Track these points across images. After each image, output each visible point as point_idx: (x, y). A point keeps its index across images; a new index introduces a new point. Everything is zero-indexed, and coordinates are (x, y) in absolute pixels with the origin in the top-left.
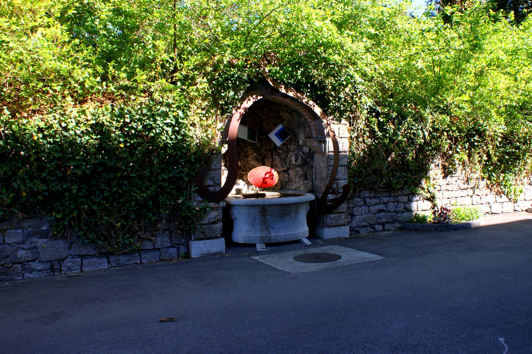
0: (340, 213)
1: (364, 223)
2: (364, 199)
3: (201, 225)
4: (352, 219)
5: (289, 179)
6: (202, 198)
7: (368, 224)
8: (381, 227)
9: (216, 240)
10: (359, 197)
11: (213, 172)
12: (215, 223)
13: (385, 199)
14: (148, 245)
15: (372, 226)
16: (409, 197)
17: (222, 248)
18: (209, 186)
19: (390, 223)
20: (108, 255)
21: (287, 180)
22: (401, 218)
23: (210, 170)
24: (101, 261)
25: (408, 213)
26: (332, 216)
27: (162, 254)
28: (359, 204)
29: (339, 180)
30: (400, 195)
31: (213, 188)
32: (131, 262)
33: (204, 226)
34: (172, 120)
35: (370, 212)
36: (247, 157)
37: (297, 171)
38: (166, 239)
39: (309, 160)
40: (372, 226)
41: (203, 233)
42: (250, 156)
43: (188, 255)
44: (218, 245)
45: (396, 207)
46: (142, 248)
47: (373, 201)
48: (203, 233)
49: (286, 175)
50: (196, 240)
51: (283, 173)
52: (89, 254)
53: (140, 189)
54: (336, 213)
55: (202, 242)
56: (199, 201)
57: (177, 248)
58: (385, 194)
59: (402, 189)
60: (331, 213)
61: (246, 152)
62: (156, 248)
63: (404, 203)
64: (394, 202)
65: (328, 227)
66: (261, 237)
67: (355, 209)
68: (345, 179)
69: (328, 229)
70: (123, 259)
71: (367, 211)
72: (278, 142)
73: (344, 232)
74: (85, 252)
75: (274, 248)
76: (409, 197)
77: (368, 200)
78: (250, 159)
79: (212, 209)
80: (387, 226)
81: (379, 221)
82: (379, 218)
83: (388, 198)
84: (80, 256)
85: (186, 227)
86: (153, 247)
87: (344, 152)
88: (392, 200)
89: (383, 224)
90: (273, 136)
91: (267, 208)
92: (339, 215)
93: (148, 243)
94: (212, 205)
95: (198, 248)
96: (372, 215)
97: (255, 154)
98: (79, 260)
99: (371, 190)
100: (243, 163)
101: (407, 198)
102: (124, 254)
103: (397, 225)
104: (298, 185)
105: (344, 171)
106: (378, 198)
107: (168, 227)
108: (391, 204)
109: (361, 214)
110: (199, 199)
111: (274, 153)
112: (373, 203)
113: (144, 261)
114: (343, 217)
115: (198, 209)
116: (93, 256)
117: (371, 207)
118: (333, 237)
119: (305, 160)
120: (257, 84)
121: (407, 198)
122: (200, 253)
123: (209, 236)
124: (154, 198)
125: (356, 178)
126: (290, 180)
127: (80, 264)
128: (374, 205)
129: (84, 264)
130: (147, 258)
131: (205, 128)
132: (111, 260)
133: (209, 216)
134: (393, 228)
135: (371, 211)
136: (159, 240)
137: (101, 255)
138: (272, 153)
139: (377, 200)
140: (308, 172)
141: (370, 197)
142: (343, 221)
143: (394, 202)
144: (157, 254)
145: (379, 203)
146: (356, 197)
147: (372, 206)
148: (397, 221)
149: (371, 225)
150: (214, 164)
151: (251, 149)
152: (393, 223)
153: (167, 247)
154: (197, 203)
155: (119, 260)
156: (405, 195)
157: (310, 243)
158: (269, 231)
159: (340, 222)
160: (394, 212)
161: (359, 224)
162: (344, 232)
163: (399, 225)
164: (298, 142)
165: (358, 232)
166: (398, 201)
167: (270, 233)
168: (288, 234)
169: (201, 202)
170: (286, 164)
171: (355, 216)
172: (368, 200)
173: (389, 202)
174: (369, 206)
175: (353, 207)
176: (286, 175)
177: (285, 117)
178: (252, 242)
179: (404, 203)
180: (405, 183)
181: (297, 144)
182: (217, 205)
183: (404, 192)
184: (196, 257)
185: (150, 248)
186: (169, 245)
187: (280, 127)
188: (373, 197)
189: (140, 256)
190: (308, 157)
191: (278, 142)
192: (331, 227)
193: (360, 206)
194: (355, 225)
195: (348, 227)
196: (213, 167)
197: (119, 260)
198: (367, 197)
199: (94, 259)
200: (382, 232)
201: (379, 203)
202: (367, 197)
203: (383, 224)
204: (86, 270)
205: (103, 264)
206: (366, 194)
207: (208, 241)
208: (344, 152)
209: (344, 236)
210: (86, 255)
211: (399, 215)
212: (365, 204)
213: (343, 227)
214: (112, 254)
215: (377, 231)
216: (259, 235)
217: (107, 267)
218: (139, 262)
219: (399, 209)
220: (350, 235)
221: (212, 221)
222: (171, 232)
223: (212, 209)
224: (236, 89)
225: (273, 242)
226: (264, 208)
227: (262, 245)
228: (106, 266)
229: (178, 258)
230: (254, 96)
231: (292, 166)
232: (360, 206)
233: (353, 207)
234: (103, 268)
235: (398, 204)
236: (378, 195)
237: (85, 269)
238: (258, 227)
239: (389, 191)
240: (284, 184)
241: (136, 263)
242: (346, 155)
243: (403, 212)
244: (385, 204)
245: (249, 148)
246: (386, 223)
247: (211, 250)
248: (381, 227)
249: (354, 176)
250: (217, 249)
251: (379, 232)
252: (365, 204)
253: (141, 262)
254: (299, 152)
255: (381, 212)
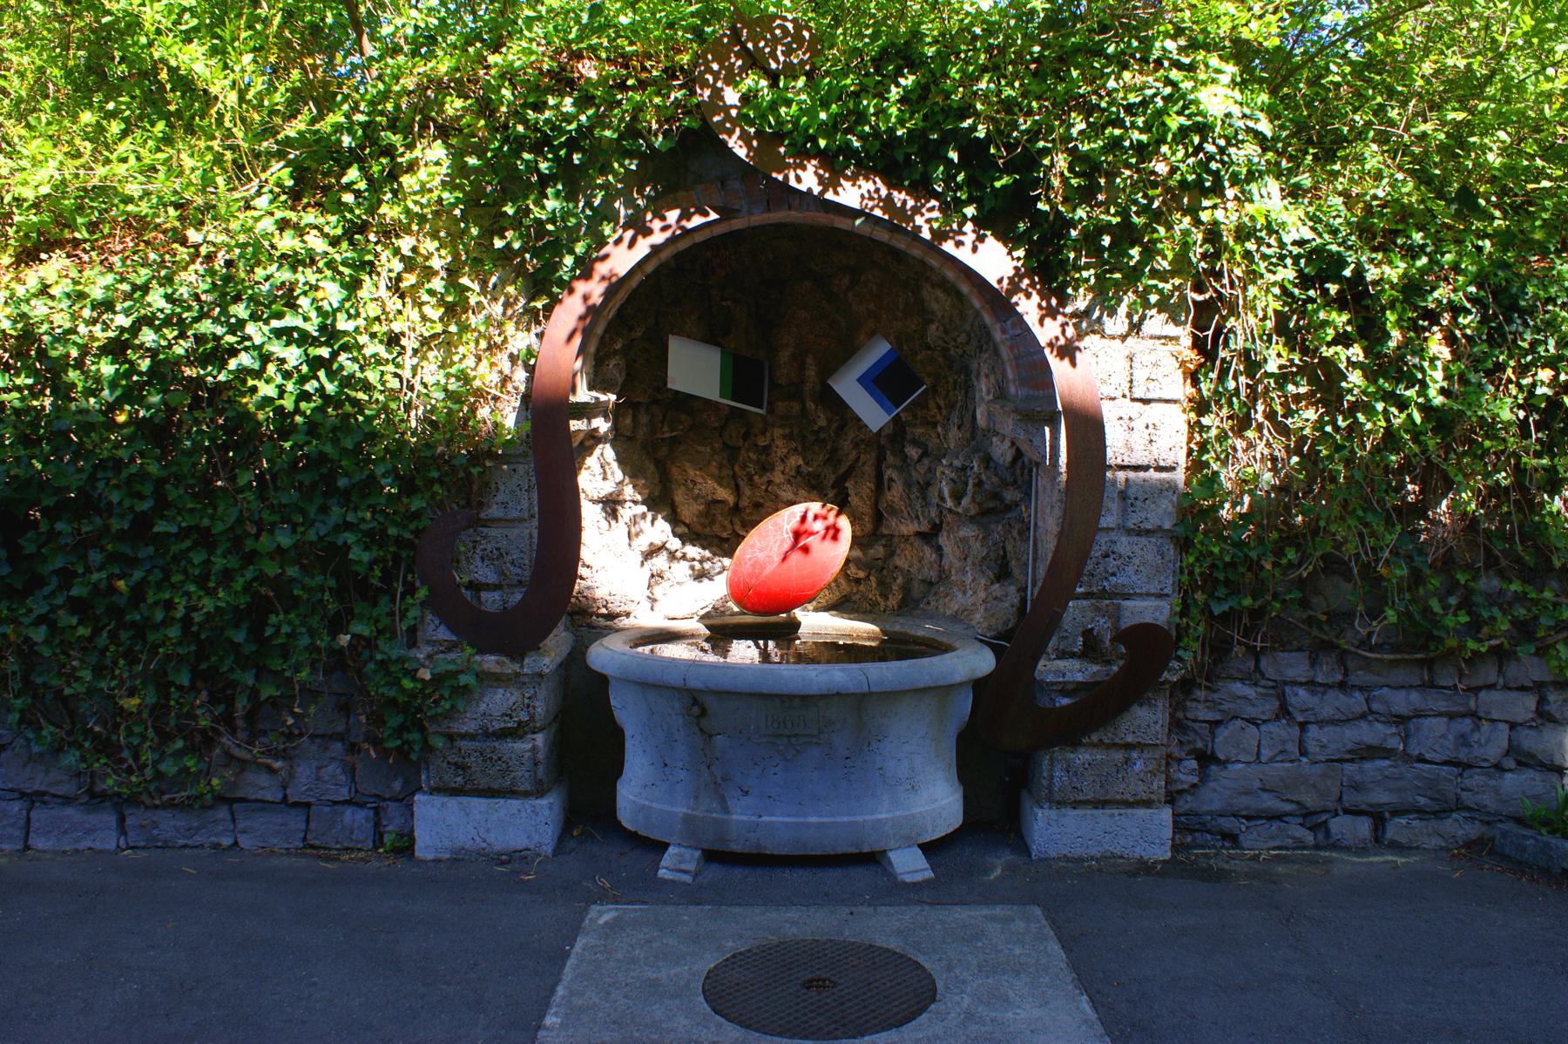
0: (1128, 747)
1: (1269, 802)
2: (1279, 689)
3: (450, 738)
4: (1204, 777)
5: (941, 570)
6: (452, 629)
7: (1288, 807)
8: (1364, 827)
9: (514, 804)
10: (1254, 677)
11: (493, 532)
12: (517, 732)
13: (1401, 702)
14: (262, 786)
15: (1313, 819)
16: (1542, 701)
17: (536, 838)
18: (476, 587)
19: (1420, 812)
20: (121, 804)
21: (933, 575)
22: (1487, 800)
23: (477, 523)
24: (93, 819)
25: (1529, 774)
26: (1082, 757)
27: (313, 825)
28: (1251, 712)
29: (1127, 597)
30: (1492, 687)
31: (496, 595)
32: (198, 839)
33: (463, 744)
34: (306, 319)
35: (1303, 753)
36: (766, 468)
37: (964, 540)
38: (333, 769)
39: (1010, 495)
40: (1313, 819)
41: (462, 768)
42: (779, 467)
43: (405, 847)
44: (528, 823)
45: (1463, 740)
46: (240, 794)
47: (1334, 704)
48: (462, 768)
49: (927, 550)
50: (434, 791)
51: (917, 542)
52: (52, 791)
53: (202, 581)
54: (1100, 744)
55: (453, 802)
56: (439, 643)
57: (376, 810)
58: (1400, 675)
59: (1501, 655)
60: (1075, 744)
61: (766, 450)
62: (291, 800)
63: (1513, 726)
64: (1452, 716)
65: (1060, 804)
66: (687, 820)
67: (1223, 734)
68: (1160, 596)
69: (1053, 814)
70: (170, 824)
71: (1293, 748)
72: (873, 414)
73: (1149, 833)
74: (38, 781)
75: (738, 873)
76: (1542, 701)
77: (1300, 697)
78: (778, 477)
79: (497, 680)
80: (1396, 829)
81: (1349, 799)
82: (1357, 787)
83: (1414, 696)
84: (23, 795)
85: (406, 742)
86: (280, 796)
87: (1159, 469)
88: (1442, 706)
89: (1379, 818)
90: (849, 388)
91: (711, 703)
92: (1119, 756)
93: (263, 779)
94: (490, 662)
95: (441, 824)
96: (1318, 769)
97: (795, 461)
98: (16, 807)
99: (1319, 649)
100: (747, 491)
101: (1530, 702)
102: (171, 805)
103: (1458, 828)
104: (970, 600)
105: (1150, 556)
106: (1361, 689)
107: (340, 728)
108: (1435, 725)
109: (1255, 757)
110: (443, 634)
111: (890, 459)
112: (1327, 711)
113: (245, 842)
114: (1139, 766)
115: (426, 674)
116: (67, 801)
117: (1313, 728)
118: (1078, 852)
119: (996, 496)
120: (686, 160)
121: (1530, 702)
122: (447, 843)
123: (483, 782)
124: (255, 613)
125: (1222, 592)
126: (943, 576)
127: (22, 822)
128: (1333, 722)
129: (35, 825)
130: (259, 834)
131: (466, 354)
132: (129, 821)
133: (483, 707)
134: (1436, 842)
135: (1312, 747)
136: (304, 772)
137: (96, 799)
138: (881, 459)
139: (1357, 702)
140: (1009, 548)
141: (1310, 684)
142: (1142, 787)
143: (1452, 716)
144: (296, 821)
145: (1363, 716)
146: (1235, 679)
147: (1321, 723)
148: (1460, 806)
149: (1306, 814)
150: (499, 498)
151: (784, 437)
152: (1439, 814)
153: (336, 803)
154: (432, 651)
155: (155, 825)
156: (1522, 689)
157: (929, 874)
158: (723, 800)
159: (1118, 790)
160: (1445, 763)
161: (1245, 801)
162: (1149, 833)
163: (1474, 830)
164: (974, 417)
165: (1232, 838)
166: (1474, 715)
167: (726, 809)
168: (809, 825)
169: (451, 647)
170: (927, 504)
171: (1223, 763)
172: (1300, 697)
173: (1419, 715)
174: (1303, 726)
175: (1215, 724)
176: (929, 554)
177: (935, 306)
178: (656, 835)
179: (1513, 726)
180: (1525, 630)
181: (967, 424)
182: (510, 667)
183: (1513, 671)
184: (430, 856)
185: (269, 797)
186: (344, 794)
187: (879, 350)
188: (1328, 686)
189: (234, 820)
190: (1005, 484)
191: (873, 414)
192: (1076, 804)
193: (1252, 721)
194: (1216, 806)
195: (1166, 814)
196: (495, 511)
197: (155, 825)
198: (1294, 683)
199: (70, 811)
200: (1363, 851)
201: (1363, 716)
202: (1294, 683)
203: (1379, 818)
204: (40, 846)
205: (101, 833)
206: (1295, 666)
207: (478, 804)
208: (1159, 469)
209: (1138, 852)
210: (44, 793)
211: (1476, 779)
212: (1284, 712)
213: (1141, 812)
214: (134, 801)
215: (1335, 847)
216: (681, 810)
217: (113, 845)
218: (226, 841)
219: (1478, 752)
220: (1175, 848)
221: (497, 726)
222: (353, 748)
223: (497, 680)
224: (572, 181)
225: (736, 847)
226: (695, 702)
227: (688, 853)
228: (108, 840)
229: (376, 848)
230: (673, 216)
231: (949, 518)
232: (1252, 721)
233: (1215, 724)
234: (98, 845)
235: (1477, 728)
236: (1359, 677)
237: (38, 842)
238: (683, 775)
239: (1428, 663)
240: (917, 589)
241: (216, 846)
242: (1171, 487)
243: (1498, 767)
244: (1400, 720)
245: (778, 432)
246: (1396, 813)
247: (491, 838)
248: (1364, 827)
249: (1210, 583)
250: (515, 839)
251: (1347, 849)
252: (1284, 712)
253: (236, 843)
254: (969, 457)
255: (1372, 758)
